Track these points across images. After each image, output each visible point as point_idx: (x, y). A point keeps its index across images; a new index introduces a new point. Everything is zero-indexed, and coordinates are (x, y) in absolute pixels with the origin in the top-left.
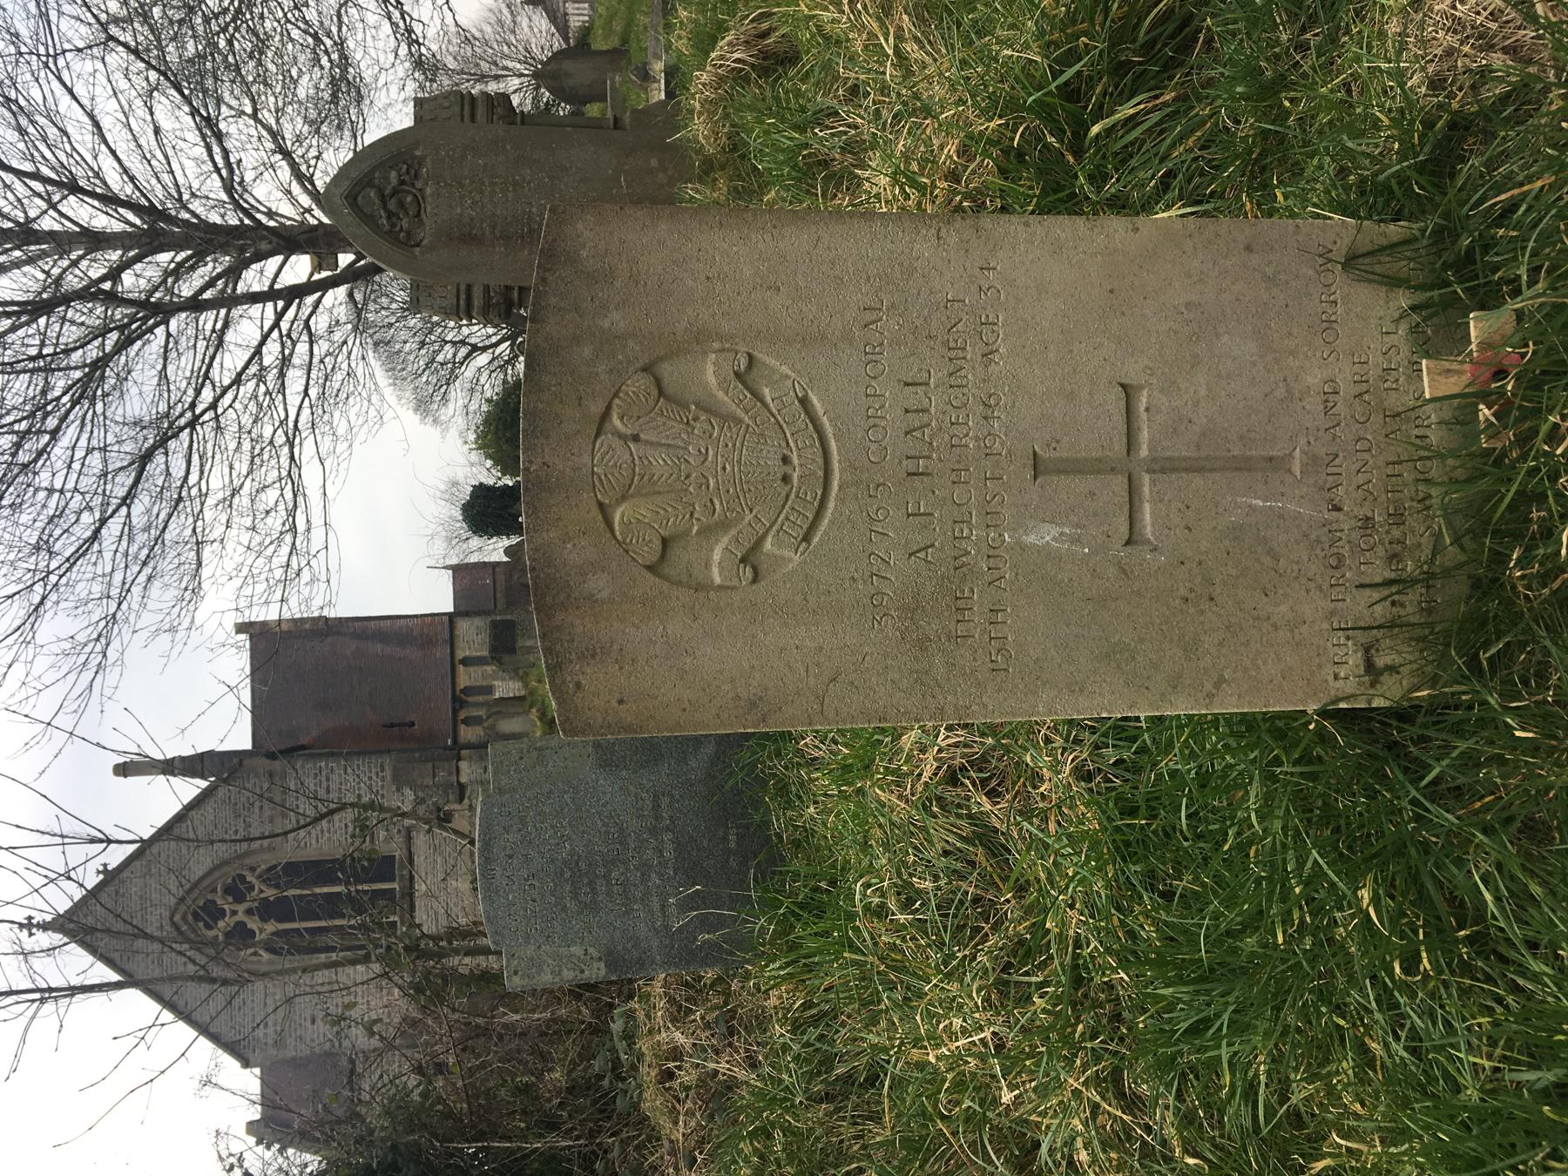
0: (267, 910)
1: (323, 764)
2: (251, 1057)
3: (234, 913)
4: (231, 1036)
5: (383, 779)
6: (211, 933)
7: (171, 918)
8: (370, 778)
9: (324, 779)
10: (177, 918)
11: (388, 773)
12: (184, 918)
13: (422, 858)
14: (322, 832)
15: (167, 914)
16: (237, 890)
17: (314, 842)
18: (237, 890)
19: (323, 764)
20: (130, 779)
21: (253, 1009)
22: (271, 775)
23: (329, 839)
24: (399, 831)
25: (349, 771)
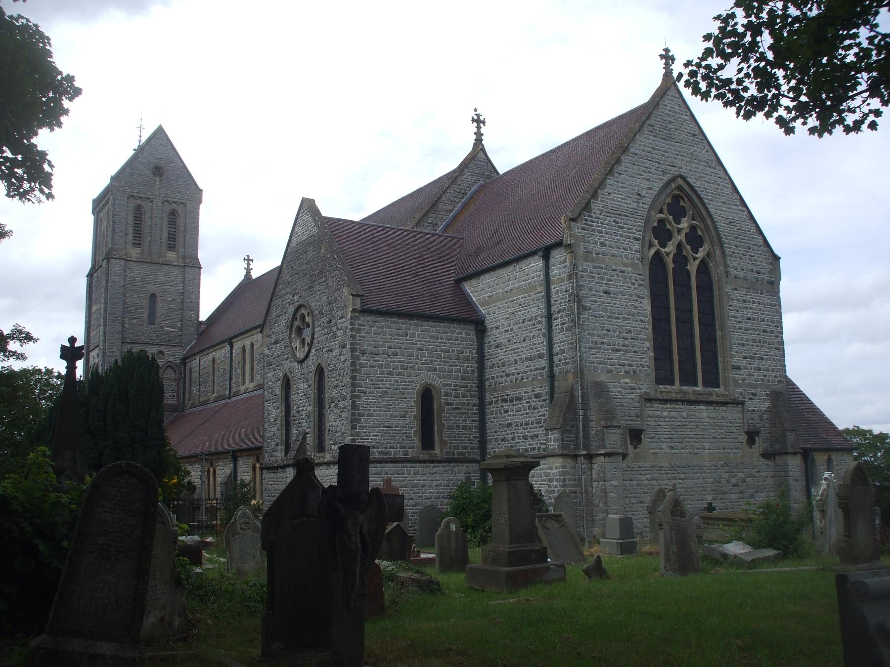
10: (680, 181)
23: (734, 327)
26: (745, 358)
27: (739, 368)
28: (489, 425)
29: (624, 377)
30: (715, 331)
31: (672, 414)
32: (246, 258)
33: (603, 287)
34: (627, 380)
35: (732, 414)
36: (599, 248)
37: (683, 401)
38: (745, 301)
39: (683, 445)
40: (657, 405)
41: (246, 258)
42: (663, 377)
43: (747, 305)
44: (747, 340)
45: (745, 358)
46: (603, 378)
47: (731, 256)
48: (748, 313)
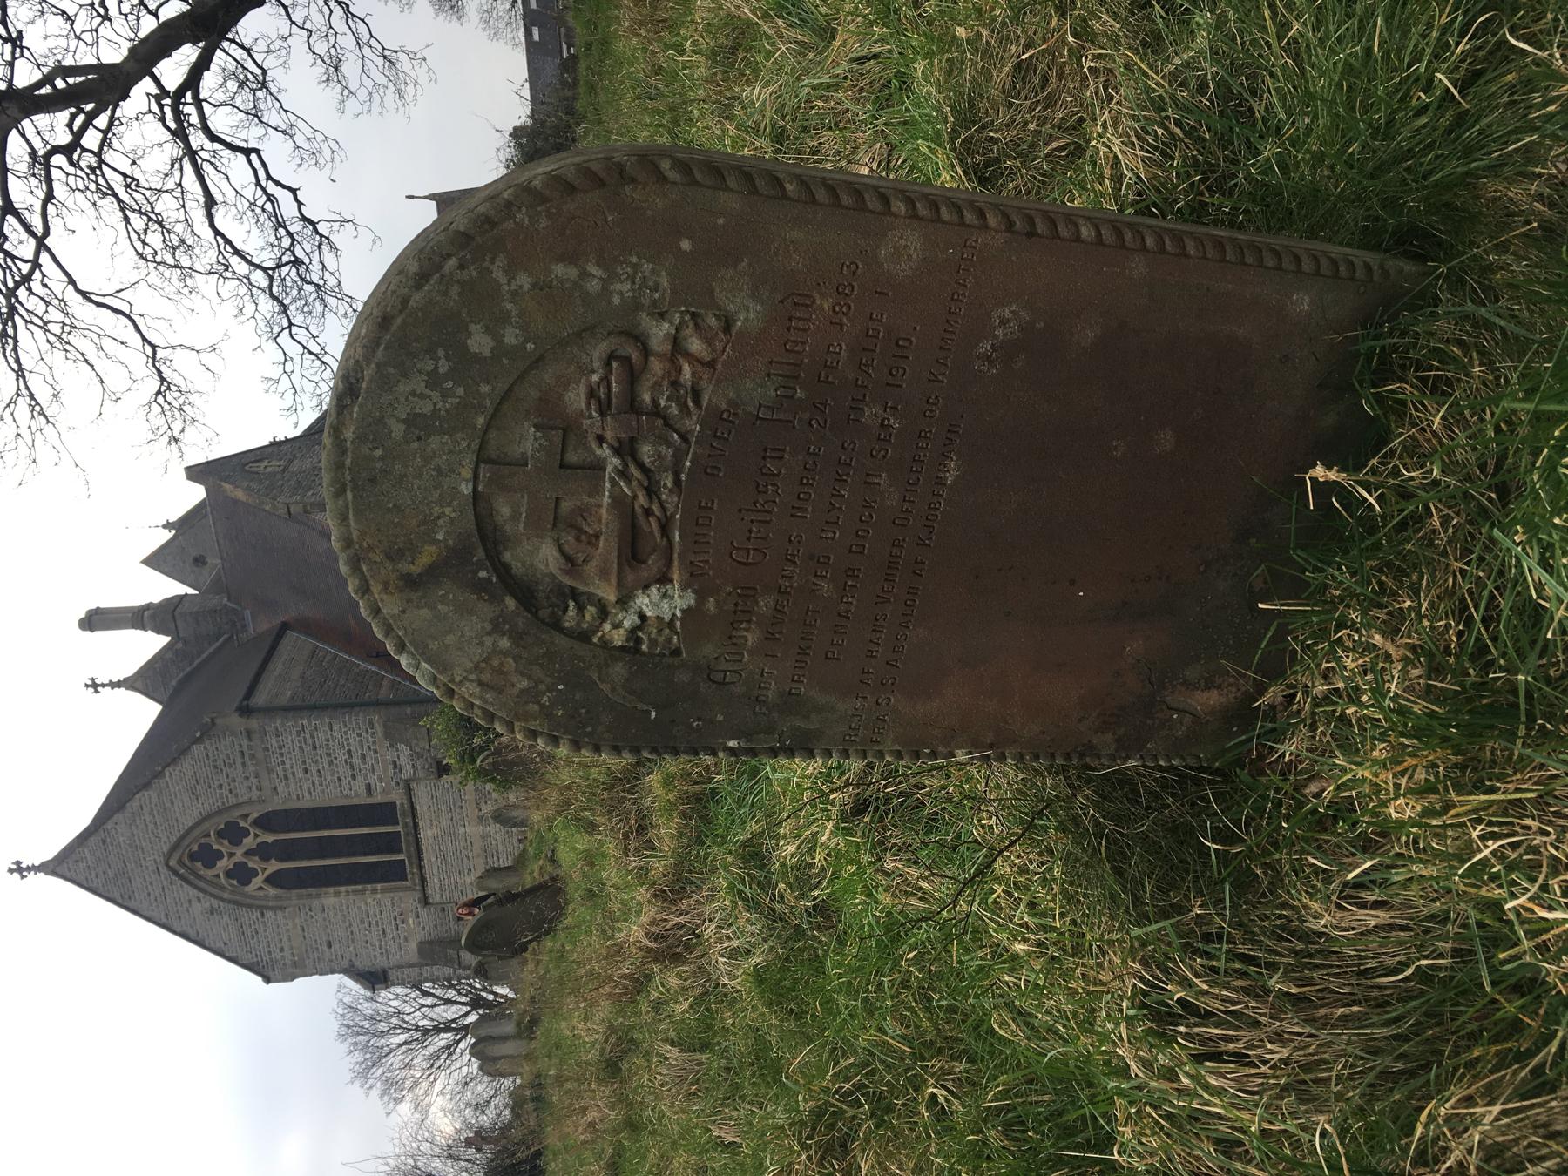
0: (263, 852)
1: (305, 722)
2: (271, 974)
3: (231, 855)
4: (248, 958)
5: (374, 735)
6: (210, 872)
7: (167, 865)
8: (359, 735)
9: (308, 736)
10: (173, 863)
11: (379, 729)
12: (180, 862)
13: (425, 808)
14: (314, 784)
15: (161, 860)
16: (233, 833)
17: (306, 794)
18: (233, 833)
19: (305, 722)
20: (97, 633)
21: (266, 937)
22: (249, 733)
23: (323, 792)
24: (398, 784)
25: (335, 727)
26: (354, 777)
27: (369, 787)
28: (306, 803)
29: (408, 924)
30: (380, 882)
31: (435, 872)
32: (90, 682)
33: (325, 948)
34: (411, 921)
35: (422, 793)
36: (287, 953)
37: (420, 860)
38: (286, 777)
39: (465, 860)
40: (429, 891)
41: (90, 682)
42: (392, 874)
43: (289, 772)
44: (332, 774)
45: (354, 777)
46: (413, 945)
47: (236, 796)
48: (299, 770)
